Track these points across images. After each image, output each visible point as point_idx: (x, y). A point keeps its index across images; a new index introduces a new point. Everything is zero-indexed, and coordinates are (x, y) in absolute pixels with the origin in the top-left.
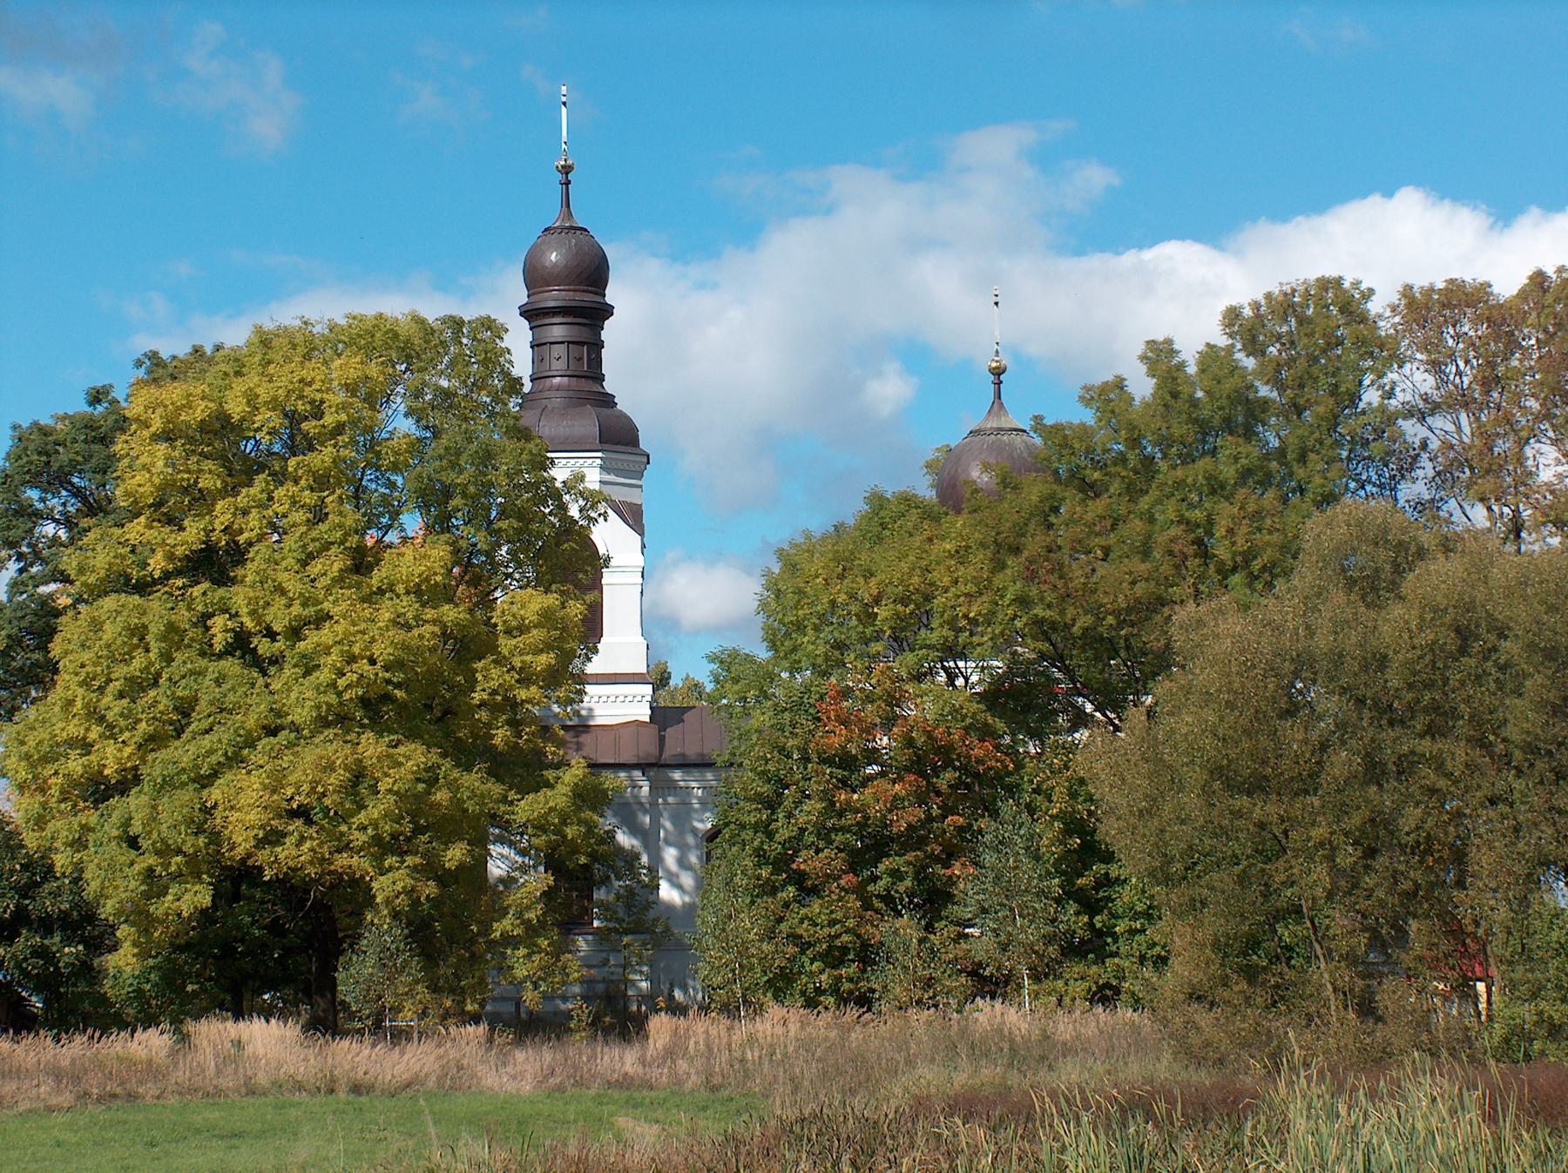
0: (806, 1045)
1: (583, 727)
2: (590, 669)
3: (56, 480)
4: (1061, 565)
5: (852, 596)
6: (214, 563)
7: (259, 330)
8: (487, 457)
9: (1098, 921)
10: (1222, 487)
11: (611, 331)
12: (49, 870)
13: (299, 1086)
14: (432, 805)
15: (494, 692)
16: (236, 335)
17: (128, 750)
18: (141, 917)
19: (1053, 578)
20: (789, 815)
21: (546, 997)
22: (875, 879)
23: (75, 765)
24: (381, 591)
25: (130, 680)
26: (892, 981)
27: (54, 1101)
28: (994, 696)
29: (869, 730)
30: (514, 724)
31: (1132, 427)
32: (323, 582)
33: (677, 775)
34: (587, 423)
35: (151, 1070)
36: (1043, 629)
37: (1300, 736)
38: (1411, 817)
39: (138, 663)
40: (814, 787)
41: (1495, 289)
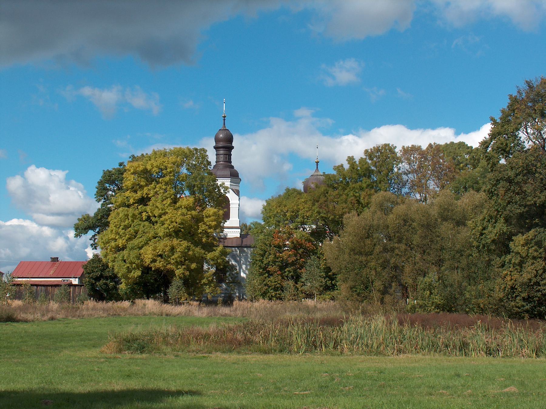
0: (265, 308)
1: (225, 238)
2: (226, 225)
3: (112, 182)
4: (328, 205)
5: (282, 211)
6: (144, 201)
7: (154, 151)
8: (202, 178)
9: (333, 282)
10: (363, 189)
11: (233, 152)
12: (108, 267)
13: (155, 314)
14: (189, 255)
15: (203, 230)
16: (149, 151)
17: (124, 241)
18: (125, 276)
19: (326, 208)
20: (266, 258)
21: (213, 296)
22: (285, 272)
23: (113, 244)
24: (179, 208)
25: (125, 226)
26: (286, 294)
27: (102, 315)
28: (313, 233)
29: (284, 240)
30: (208, 237)
31: (344, 175)
32: (166, 205)
33: (245, 249)
34: (227, 172)
35: (124, 310)
36: (323, 219)
37: (369, 243)
38: (392, 261)
39: (127, 222)
40: (272, 252)
41: (422, 147)
